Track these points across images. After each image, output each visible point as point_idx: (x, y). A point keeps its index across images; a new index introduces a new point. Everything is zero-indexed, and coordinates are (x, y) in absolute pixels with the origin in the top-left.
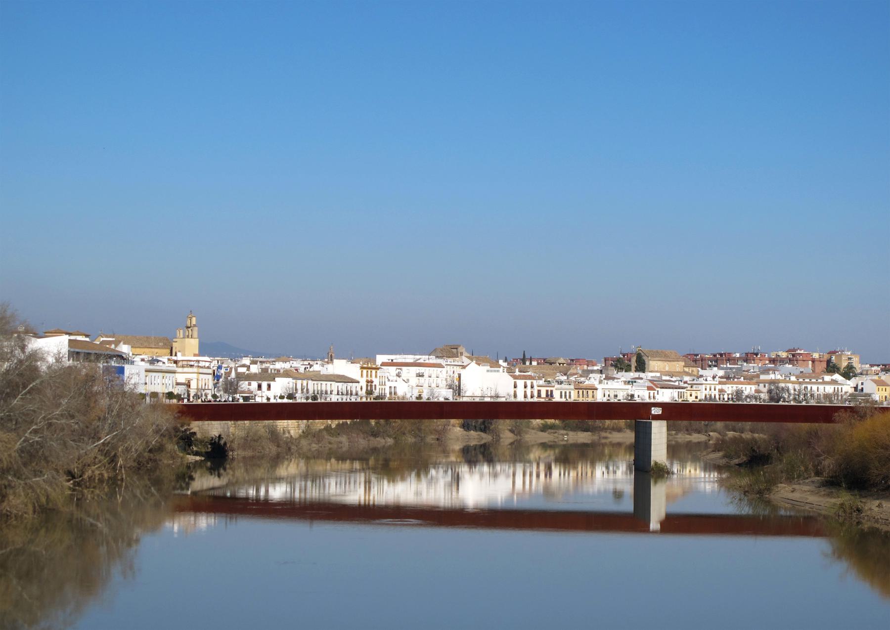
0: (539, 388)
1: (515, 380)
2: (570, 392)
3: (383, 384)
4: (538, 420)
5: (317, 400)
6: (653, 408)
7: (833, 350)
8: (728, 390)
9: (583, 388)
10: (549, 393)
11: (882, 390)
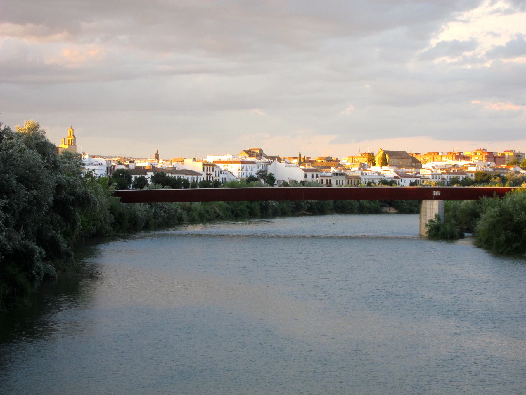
0: (322, 178)
1: (306, 173)
2: (343, 181)
3: (218, 176)
4: (465, 201)
5: (197, 188)
6: (434, 192)
8: (448, 179)
10: (329, 182)
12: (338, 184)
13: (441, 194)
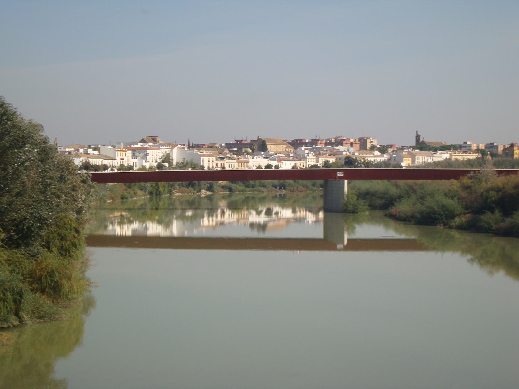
5: (403, 168)
7: (338, 136)
9: (241, 161)
11: (407, 160)
12: (230, 167)
13: (344, 175)
